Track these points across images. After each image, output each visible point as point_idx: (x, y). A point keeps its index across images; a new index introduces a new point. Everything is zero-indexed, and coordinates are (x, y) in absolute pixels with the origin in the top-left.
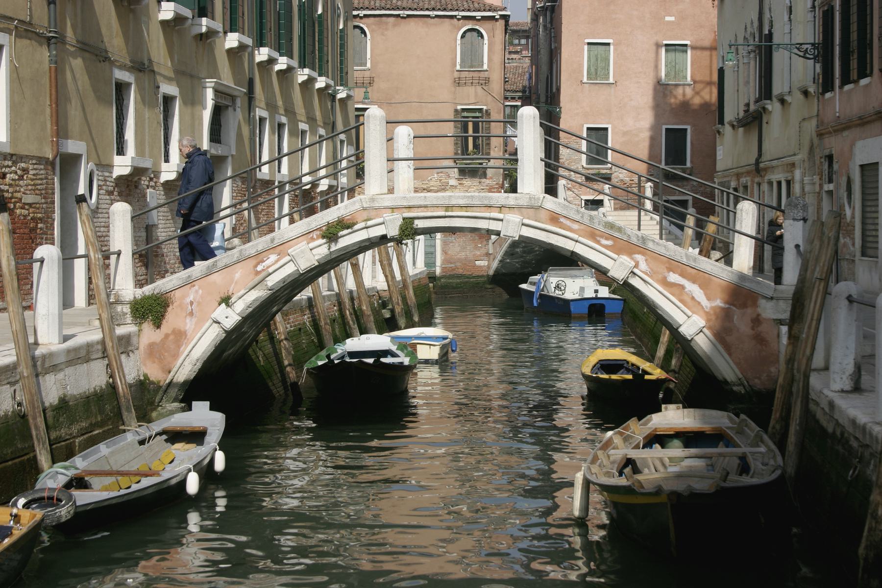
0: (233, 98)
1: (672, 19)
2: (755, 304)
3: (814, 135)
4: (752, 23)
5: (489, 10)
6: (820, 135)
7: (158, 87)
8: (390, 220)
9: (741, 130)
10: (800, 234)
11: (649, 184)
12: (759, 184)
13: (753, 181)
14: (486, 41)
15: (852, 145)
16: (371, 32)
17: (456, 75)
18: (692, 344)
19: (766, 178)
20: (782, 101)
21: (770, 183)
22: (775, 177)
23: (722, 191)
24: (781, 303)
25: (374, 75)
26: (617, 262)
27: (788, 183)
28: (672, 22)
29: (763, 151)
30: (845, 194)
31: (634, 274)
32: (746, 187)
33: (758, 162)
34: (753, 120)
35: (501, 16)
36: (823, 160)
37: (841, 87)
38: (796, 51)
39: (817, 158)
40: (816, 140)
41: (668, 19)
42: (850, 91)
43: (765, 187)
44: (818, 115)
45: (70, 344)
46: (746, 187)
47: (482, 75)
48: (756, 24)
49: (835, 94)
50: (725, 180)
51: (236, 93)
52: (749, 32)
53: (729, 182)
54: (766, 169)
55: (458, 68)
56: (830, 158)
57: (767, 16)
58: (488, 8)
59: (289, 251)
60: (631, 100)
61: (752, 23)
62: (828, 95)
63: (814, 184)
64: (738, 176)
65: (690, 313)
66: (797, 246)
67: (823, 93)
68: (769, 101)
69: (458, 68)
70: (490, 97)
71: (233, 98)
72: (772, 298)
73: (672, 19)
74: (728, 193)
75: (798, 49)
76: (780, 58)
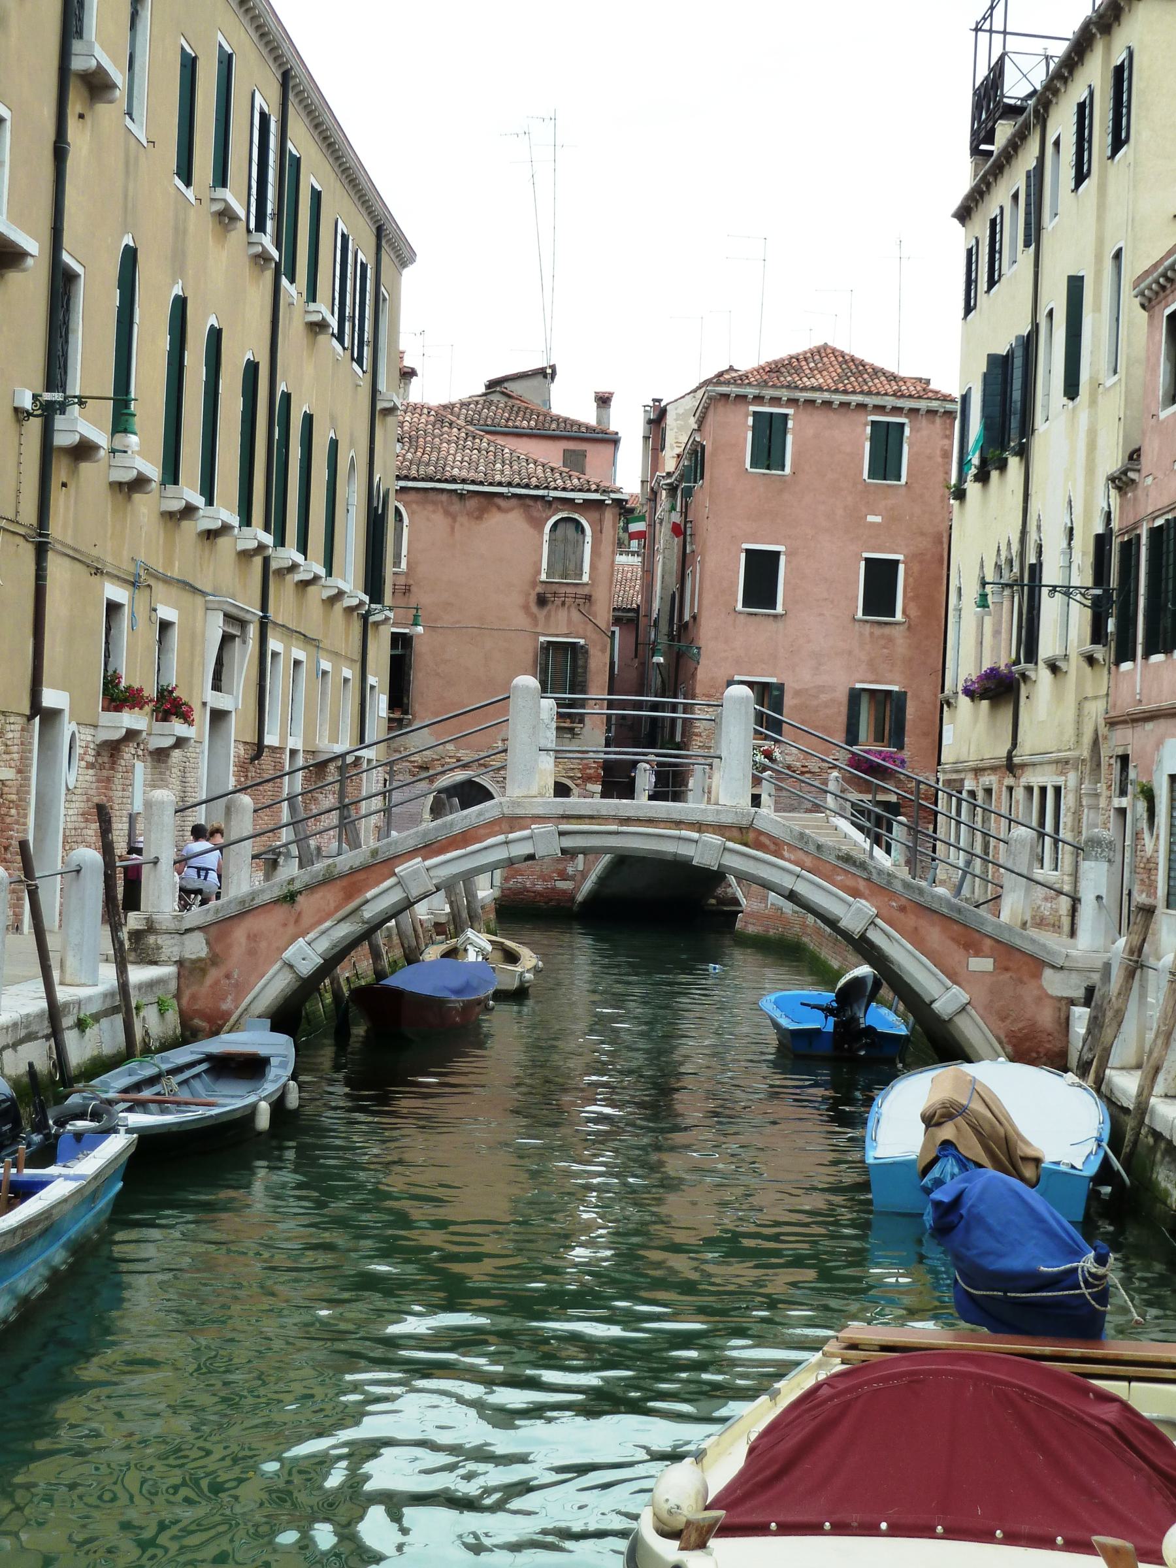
0: (243, 624)
1: (878, 519)
2: (1037, 975)
3: (1101, 722)
4: (1009, 543)
5: (596, 491)
6: (1112, 723)
7: (155, 610)
8: (540, 833)
9: (985, 704)
10: (1104, 880)
11: (835, 774)
12: (1010, 789)
13: (1000, 782)
14: (588, 538)
15: (1159, 744)
16: (411, 514)
17: (539, 589)
18: (950, 1027)
19: (1023, 781)
20: (1054, 668)
21: (1029, 789)
22: (1036, 778)
23: (951, 796)
24: (1074, 975)
25: (411, 582)
26: (853, 908)
27: (1058, 790)
28: (878, 524)
29: (1019, 740)
30: (1145, 815)
31: (876, 925)
32: (989, 791)
33: (1010, 757)
34: (1000, 689)
35: (613, 500)
36: (1113, 761)
37: (1146, 656)
38: (1079, 597)
39: (1104, 761)
40: (1103, 730)
41: (870, 518)
42: (1159, 664)
43: (1019, 794)
44: (1107, 695)
45: (619, 988)
46: (989, 791)
47: (580, 591)
48: (1015, 547)
49: (1135, 665)
50: (954, 776)
51: (248, 617)
52: (1003, 558)
53: (962, 780)
54: (1023, 766)
55: (543, 577)
56: (1124, 760)
57: (1032, 537)
58: (593, 487)
59: (397, 870)
60: (809, 642)
61: (1009, 543)
62: (1126, 666)
63: (1097, 795)
64: (978, 771)
65: (949, 983)
66: (1099, 898)
67: (1117, 663)
68: (1031, 666)
69: (543, 577)
70: (590, 626)
71: (243, 624)
72: (1062, 968)
73: (878, 519)
74: (959, 800)
75: (1083, 595)
76: (1050, 607)
